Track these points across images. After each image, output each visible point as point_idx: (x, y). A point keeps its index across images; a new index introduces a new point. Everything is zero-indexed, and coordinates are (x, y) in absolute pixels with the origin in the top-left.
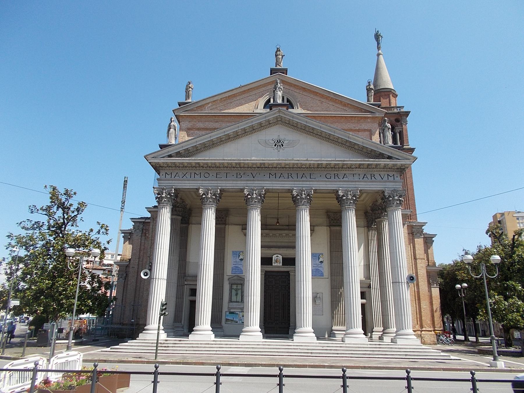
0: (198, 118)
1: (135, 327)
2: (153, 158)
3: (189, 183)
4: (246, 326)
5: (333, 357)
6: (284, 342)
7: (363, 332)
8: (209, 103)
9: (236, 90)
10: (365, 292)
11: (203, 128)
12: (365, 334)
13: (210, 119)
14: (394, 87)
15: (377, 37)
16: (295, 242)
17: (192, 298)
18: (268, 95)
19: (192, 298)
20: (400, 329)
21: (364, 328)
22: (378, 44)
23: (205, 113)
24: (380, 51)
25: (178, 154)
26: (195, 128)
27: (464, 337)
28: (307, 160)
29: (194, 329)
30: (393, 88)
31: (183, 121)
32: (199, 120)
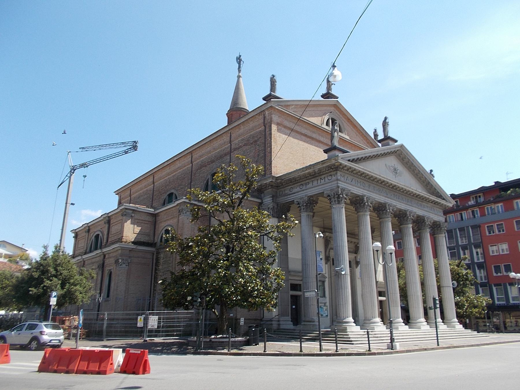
1: (162, 316)
3: (356, 189)
4: (396, 318)
5: (410, 341)
7: (354, 321)
8: (293, 105)
11: (288, 127)
12: (428, 323)
13: (293, 120)
14: (249, 108)
15: (239, 60)
18: (328, 115)
20: (372, 317)
22: (239, 67)
23: (289, 112)
24: (240, 74)
25: (353, 161)
26: (282, 125)
28: (416, 190)
30: (248, 109)
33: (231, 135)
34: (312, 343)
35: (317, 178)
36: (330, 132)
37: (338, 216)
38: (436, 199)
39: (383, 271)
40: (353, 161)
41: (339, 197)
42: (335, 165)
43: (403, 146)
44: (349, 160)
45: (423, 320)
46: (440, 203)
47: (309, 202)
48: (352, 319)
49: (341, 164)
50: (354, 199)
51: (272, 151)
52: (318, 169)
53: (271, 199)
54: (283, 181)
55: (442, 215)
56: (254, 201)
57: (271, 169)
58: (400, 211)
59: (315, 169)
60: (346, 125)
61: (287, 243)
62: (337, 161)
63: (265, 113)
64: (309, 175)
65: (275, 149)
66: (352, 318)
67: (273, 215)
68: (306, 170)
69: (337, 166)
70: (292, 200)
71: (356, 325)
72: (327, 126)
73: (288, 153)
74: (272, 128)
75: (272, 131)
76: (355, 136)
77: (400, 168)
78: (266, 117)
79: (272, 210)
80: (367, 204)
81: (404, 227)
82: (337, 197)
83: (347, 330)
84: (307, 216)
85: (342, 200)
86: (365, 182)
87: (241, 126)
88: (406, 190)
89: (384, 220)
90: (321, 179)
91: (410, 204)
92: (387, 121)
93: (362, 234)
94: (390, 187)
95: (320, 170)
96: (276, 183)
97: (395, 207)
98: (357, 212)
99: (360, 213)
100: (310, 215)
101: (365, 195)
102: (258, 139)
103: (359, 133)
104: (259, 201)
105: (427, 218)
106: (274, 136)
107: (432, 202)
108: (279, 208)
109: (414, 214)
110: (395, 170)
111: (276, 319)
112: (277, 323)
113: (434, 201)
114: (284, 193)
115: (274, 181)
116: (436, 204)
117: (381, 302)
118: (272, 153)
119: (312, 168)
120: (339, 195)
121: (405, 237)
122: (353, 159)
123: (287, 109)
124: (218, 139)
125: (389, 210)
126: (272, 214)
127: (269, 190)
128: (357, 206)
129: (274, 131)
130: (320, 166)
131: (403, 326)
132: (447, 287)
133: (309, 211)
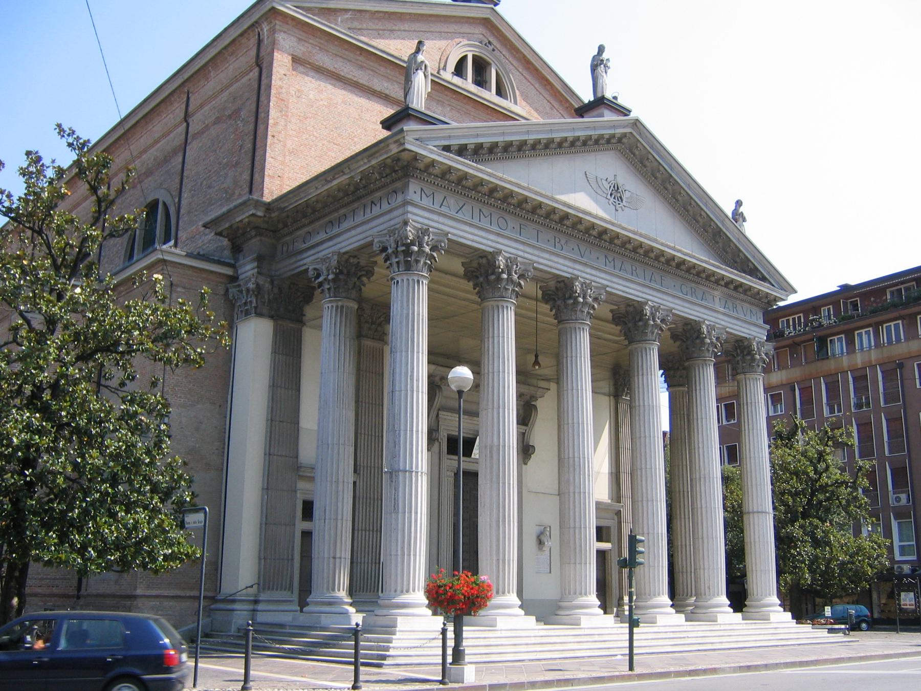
0: (321, 39)
2: (417, 140)
4: (581, 594)
6: (474, 631)
7: (520, 603)
8: (346, 11)
9: (411, 4)
10: (312, 521)
12: (605, 608)
13: (347, 53)
16: (478, 404)
17: (306, 525)
19: (306, 525)
21: (672, 595)
25: (461, 151)
27: (826, 608)
29: (308, 600)
31: (285, 32)
32: (322, 46)
33: (188, 98)
34: (296, 666)
35: (363, 201)
36: (405, 65)
37: (402, 306)
38: (736, 275)
39: (611, 474)
40: (461, 151)
41: (408, 253)
42: (398, 160)
43: (638, 124)
44: (447, 148)
45: (665, 599)
46: (750, 288)
47: (345, 271)
48: (517, 599)
49: (416, 157)
50: (475, 265)
51: (269, 133)
52: (361, 172)
53: (255, 264)
54: (284, 215)
55: (761, 321)
56: (212, 272)
57: (263, 182)
58: (686, 324)
59: (353, 174)
60: (515, 78)
61: (298, 390)
62: (401, 148)
63: (262, 30)
64: (341, 194)
65: (280, 127)
66: (776, 596)
67: (258, 311)
68: (334, 179)
69: (405, 163)
70: (304, 268)
71: (525, 615)
72: (498, 98)
73: (325, 142)
74: (274, 70)
75: (274, 77)
76: (548, 108)
77: (632, 184)
78: (263, 40)
79: (256, 296)
80: (581, 300)
81: (636, 348)
82: (403, 251)
83: (396, 627)
84: (336, 310)
85: (417, 261)
86: (507, 217)
87: (210, 72)
88: (694, 267)
89: (568, 325)
90: (372, 202)
91: (658, 287)
92: (605, 56)
93: (486, 362)
94: (509, 204)
95: (365, 176)
96: (266, 219)
97: (669, 313)
98: (559, 322)
99: (486, 304)
100: (347, 307)
101: (577, 277)
102: (243, 104)
103: (561, 102)
104: (229, 271)
105: (652, 307)
106: (279, 93)
107: (727, 285)
108: (276, 290)
109: (665, 313)
110: (616, 193)
111: (247, 595)
112: (251, 607)
113: (732, 281)
114: (291, 248)
115: (260, 214)
116: (741, 290)
117: (601, 554)
118: (269, 137)
119: (347, 171)
120: (408, 246)
121: (636, 378)
122: (479, 148)
123: (328, 20)
124: (163, 112)
125: (654, 320)
126: (256, 308)
127: (254, 240)
128: (629, 328)
129: (281, 79)
130: (364, 165)
131: (779, 612)
132: (758, 512)
133: (344, 295)
